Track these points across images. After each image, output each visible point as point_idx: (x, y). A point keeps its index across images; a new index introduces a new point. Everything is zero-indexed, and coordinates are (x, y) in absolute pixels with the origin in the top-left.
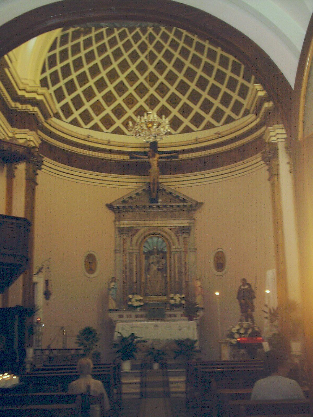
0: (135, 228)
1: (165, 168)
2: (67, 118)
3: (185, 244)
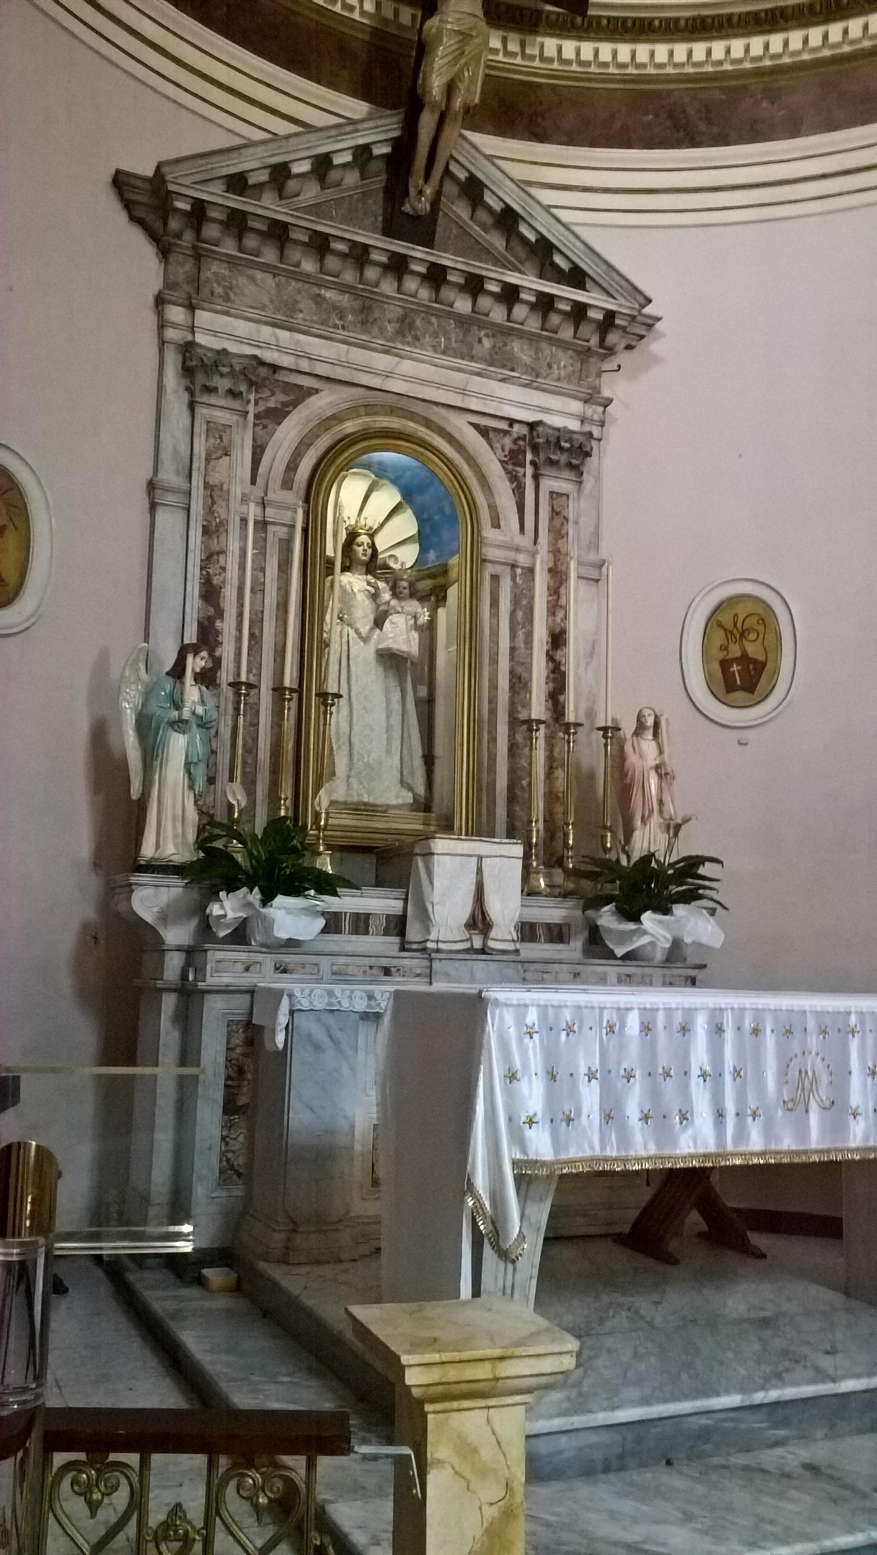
0: (284, 377)
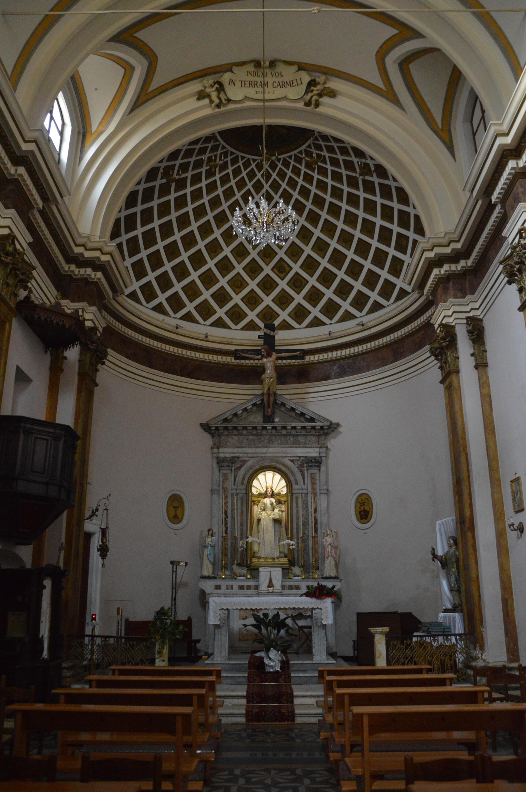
1: (284, 376)
2: (148, 302)
3: (313, 483)
